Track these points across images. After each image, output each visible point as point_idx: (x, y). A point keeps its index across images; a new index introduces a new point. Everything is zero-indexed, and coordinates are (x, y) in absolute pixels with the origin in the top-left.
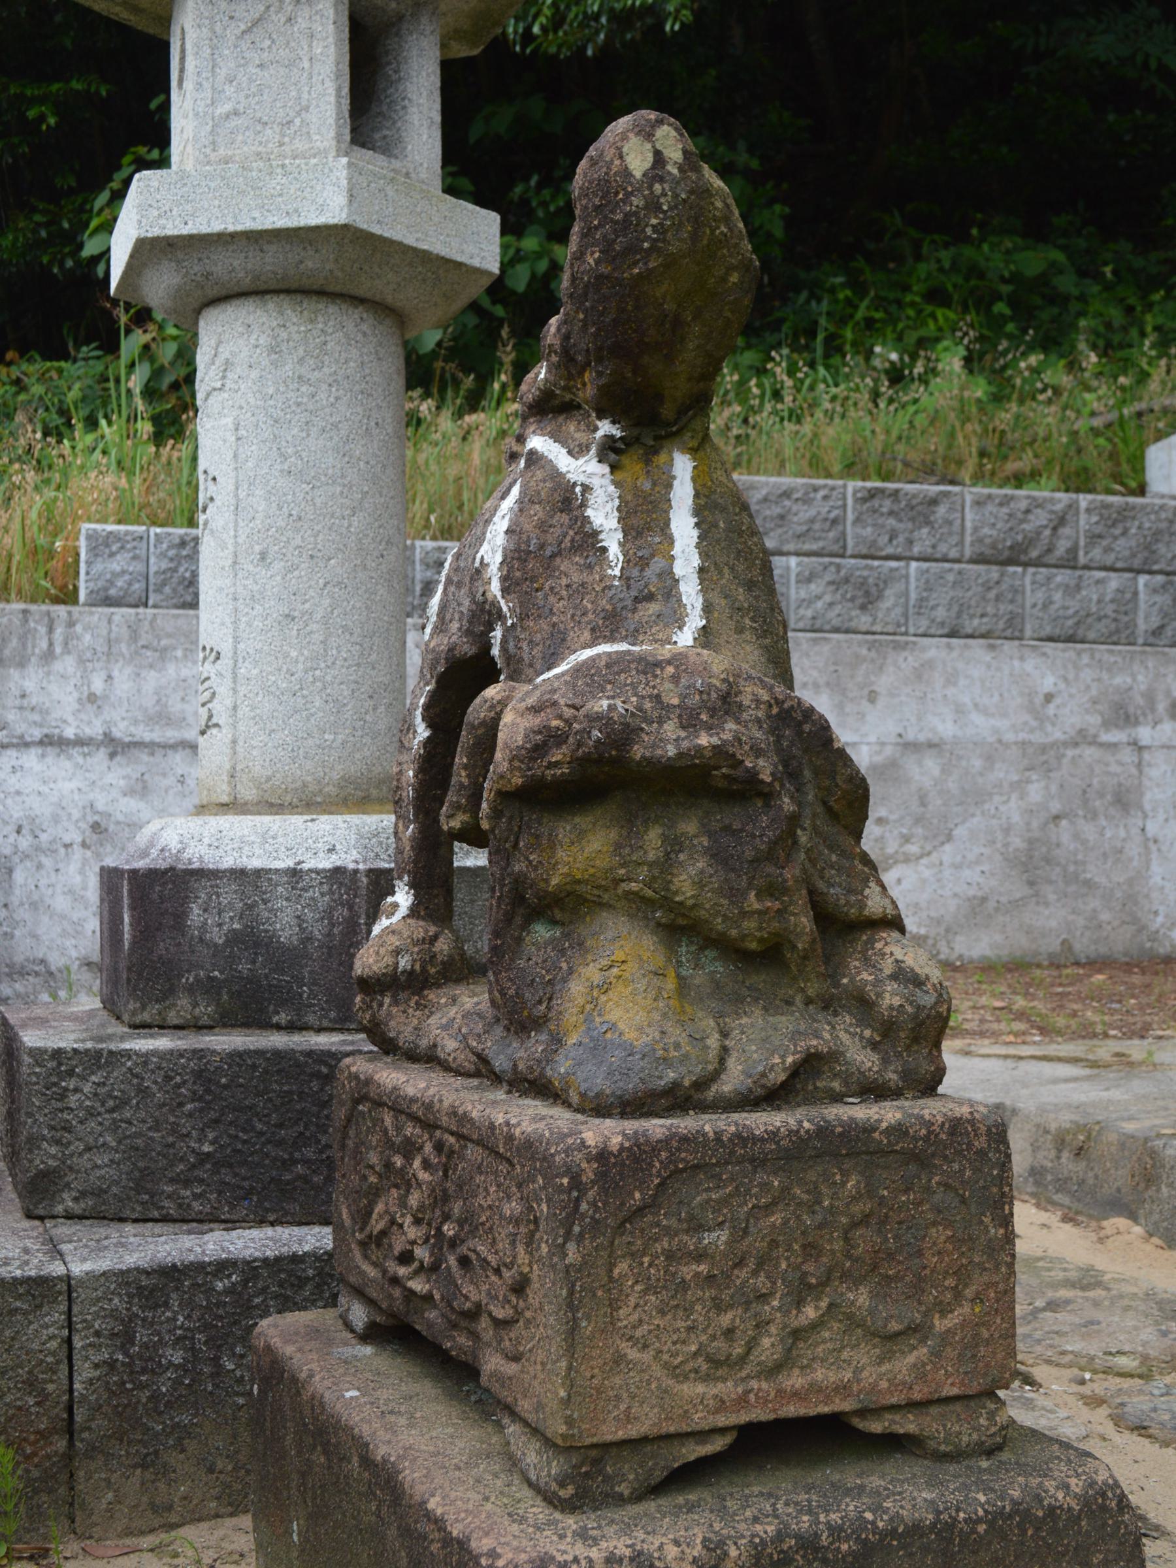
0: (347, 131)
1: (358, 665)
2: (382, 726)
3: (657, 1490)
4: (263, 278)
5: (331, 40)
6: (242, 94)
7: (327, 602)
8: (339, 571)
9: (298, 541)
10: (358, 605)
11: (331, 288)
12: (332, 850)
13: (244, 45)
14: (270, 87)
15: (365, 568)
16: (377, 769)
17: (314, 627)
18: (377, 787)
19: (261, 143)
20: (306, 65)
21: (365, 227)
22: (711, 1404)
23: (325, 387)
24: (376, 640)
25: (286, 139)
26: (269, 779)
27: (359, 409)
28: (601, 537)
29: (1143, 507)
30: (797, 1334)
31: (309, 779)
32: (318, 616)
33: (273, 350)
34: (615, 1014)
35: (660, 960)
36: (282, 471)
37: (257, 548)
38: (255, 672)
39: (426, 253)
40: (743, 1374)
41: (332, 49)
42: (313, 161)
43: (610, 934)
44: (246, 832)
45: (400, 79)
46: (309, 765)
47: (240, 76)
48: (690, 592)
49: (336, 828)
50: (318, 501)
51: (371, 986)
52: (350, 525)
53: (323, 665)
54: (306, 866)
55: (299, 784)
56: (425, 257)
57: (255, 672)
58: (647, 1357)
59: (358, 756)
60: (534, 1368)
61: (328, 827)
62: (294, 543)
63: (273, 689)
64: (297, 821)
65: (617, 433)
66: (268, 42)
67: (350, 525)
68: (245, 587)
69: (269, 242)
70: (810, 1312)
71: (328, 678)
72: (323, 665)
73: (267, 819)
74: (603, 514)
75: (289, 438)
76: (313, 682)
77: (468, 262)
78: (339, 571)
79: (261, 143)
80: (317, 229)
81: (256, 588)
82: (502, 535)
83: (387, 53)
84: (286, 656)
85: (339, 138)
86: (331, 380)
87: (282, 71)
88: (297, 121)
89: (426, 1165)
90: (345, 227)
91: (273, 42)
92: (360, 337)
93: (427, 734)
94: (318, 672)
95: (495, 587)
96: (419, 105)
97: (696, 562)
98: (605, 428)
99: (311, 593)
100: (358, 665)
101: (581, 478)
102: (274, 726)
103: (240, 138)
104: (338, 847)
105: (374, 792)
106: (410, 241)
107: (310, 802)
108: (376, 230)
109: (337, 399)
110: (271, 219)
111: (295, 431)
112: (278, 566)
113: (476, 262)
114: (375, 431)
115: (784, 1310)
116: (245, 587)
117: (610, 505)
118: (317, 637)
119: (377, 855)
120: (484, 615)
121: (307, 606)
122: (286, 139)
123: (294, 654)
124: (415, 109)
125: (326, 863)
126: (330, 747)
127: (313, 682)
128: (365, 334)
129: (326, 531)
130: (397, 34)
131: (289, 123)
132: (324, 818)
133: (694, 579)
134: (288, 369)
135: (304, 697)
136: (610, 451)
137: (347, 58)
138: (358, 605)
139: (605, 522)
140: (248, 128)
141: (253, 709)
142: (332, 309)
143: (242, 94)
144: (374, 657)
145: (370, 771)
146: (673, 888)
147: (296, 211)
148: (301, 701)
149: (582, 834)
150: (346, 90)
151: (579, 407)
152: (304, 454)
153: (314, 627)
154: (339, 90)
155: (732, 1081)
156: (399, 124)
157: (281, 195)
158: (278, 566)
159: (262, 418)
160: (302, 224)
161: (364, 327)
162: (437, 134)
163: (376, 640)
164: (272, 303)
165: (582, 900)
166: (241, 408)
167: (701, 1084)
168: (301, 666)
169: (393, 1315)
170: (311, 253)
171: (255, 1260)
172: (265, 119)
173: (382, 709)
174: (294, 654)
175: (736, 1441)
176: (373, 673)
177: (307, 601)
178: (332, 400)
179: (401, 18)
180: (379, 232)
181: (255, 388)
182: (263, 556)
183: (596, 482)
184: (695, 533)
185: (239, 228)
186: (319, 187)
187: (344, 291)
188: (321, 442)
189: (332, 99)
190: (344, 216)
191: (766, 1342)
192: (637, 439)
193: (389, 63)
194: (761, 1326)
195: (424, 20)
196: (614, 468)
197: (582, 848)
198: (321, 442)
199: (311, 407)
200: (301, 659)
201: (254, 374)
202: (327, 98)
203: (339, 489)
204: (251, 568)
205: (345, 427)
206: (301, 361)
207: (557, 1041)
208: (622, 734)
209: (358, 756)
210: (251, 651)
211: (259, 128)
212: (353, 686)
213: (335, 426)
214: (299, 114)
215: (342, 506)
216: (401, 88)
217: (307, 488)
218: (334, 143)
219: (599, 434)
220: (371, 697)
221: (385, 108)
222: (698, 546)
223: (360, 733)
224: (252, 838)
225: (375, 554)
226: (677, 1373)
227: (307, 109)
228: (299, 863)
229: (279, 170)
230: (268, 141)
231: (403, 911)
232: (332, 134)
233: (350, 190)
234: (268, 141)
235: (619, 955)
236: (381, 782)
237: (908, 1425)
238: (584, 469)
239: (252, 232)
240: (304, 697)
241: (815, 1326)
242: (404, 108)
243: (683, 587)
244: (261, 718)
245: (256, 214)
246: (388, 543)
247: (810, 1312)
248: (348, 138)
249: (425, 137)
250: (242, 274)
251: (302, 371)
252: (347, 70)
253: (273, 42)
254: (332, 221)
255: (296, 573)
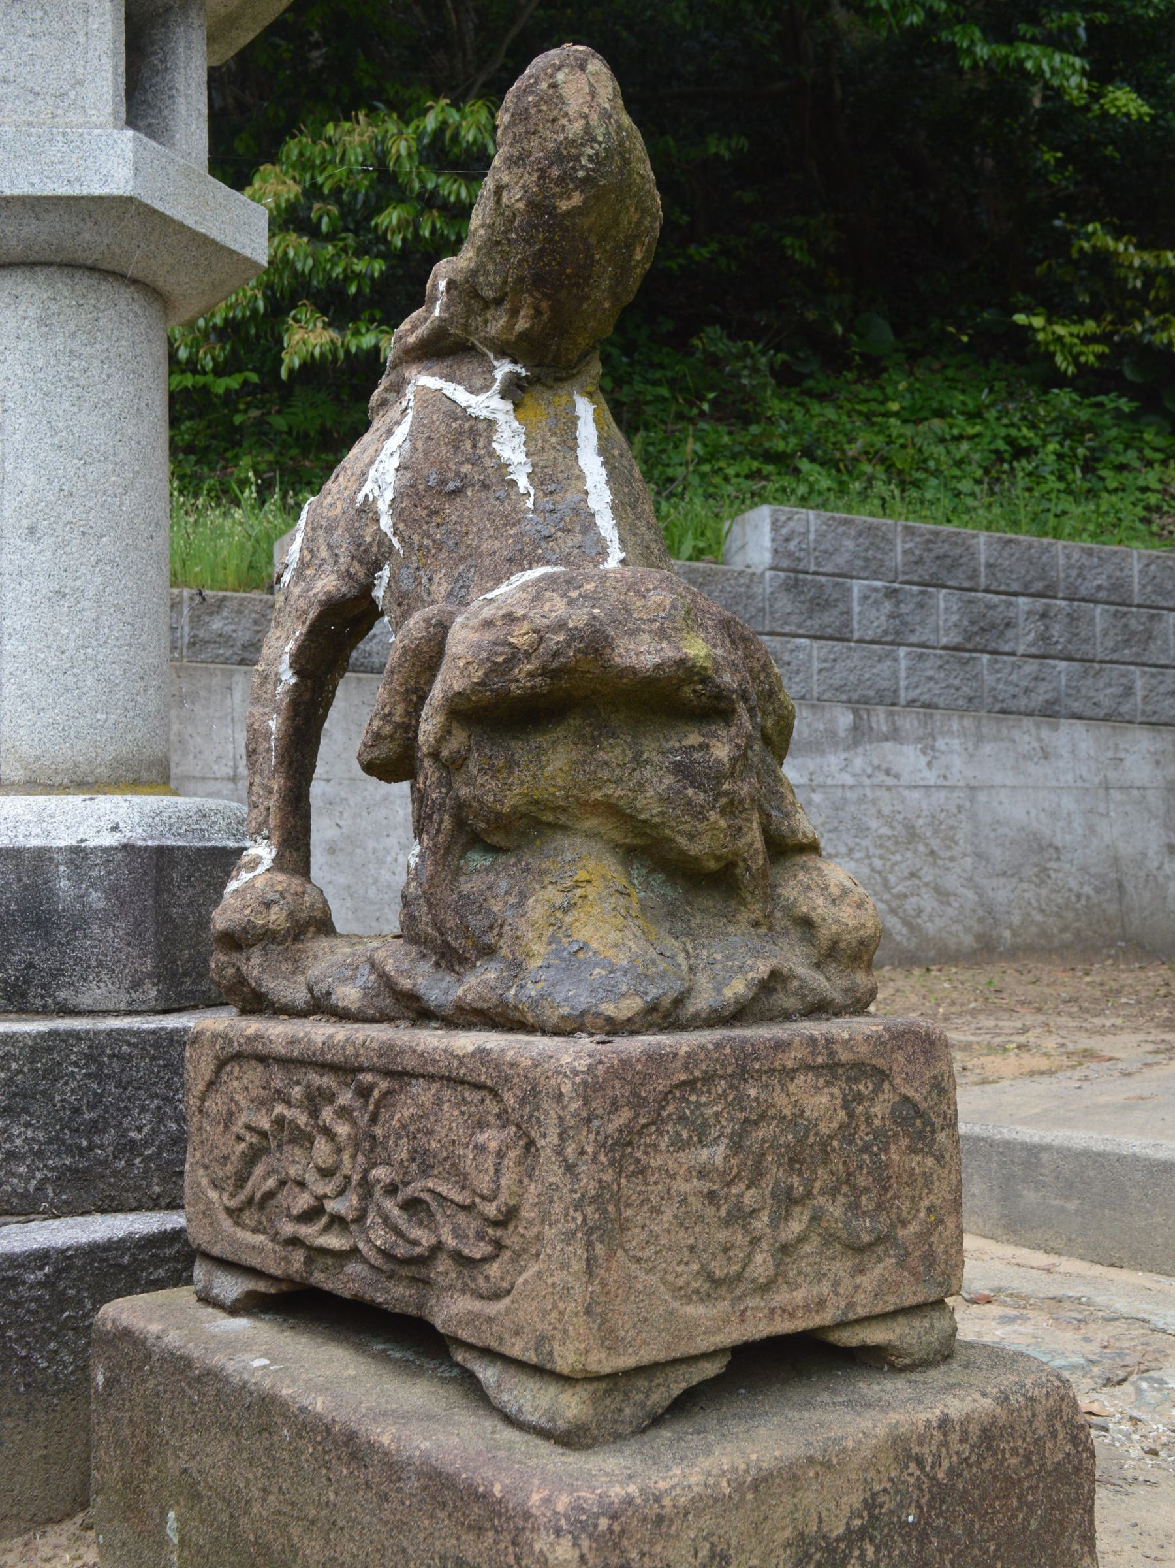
0: (123, 109)
1: (130, 645)
2: (152, 708)
3: (657, 1420)
4: (36, 248)
5: (108, 17)
6: (12, 63)
7: (98, 580)
8: (111, 549)
9: (69, 517)
10: (130, 584)
11: (104, 265)
12: (115, 828)
13: (15, 13)
14: (43, 58)
15: (136, 548)
16: (148, 752)
17: (87, 604)
18: (148, 770)
19: (32, 113)
20: (82, 40)
21: (149, 202)
22: (719, 1325)
23: (96, 363)
24: (147, 621)
25: (60, 112)
26: (38, 759)
27: (131, 389)
28: (510, 469)
29: (724, 573)
30: (785, 1249)
31: (81, 759)
32: (90, 593)
33: (42, 322)
34: (584, 934)
35: (621, 881)
36: (53, 445)
37: (25, 523)
38: (22, 649)
39: (205, 237)
40: (738, 1292)
41: (109, 26)
42: (97, 132)
43: (568, 856)
44: (20, 811)
45: (167, 69)
46: (81, 745)
47: (10, 44)
48: (606, 525)
49: (117, 806)
50: (90, 478)
51: (234, 941)
52: (122, 504)
53: (95, 643)
54: (91, 844)
55: (70, 763)
56: (203, 241)
57: (22, 649)
58: (654, 1279)
59: (129, 737)
60: (540, 1298)
61: (108, 806)
62: (65, 519)
63: (42, 666)
64: (75, 801)
65: (524, 373)
66: (40, 14)
67: (122, 504)
68: (11, 562)
69: (46, 211)
70: (796, 1227)
71: (100, 657)
72: (95, 643)
73: (42, 799)
74: (510, 447)
75: (60, 413)
76: (85, 661)
77: (241, 251)
78: (111, 549)
79: (32, 113)
80: (101, 198)
81: (23, 563)
82: (393, 472)
83: (152, 43)
84: (57, 633)
85: (115, 113)
86: (103, 357)
87: (55, 43)
88: (72, 94)
89: (344, 1113)
90: (130, 199)
91: (46, 13)
92: (131, 316)
93: (293, 681)
94: (90, 651)
95: (386, 523)
96: (187, 96)
97: (608, 498)
98: (503, 369)
99: (83, 569)
100: (130, 645)
101: (484, 413)
102: (43, 705)
103: (10, 106)
104: (122, 825)
105: (145, 775)
106: (189, 222)
107: (84, 784)
108: (158, 206)
109: (109, 376)
110: (52, 186)
111: (67, 405)
112: (48, 541)
113: (247, 252)
114: (146, 412)
115: (774, 1225)
116: (11, 562)
117: (517, 440)
118: (89, 615)
119: (161, 834)
120: (371, 558)
121: (78, 583)
122: (60, 112)
123: (65, 631)
124: (182, 100)
125: (110, 840)
126: (102, 726)
127: (85, 661)
128: (136, 314)
129: (98, 508)
130: (163, 25)
131: (62, 95)
132: (101, 797)
133: (608, 514)
134: (59, 342)
135: (75, 675)
136: (514, 391)
137: (123, 37)
138: (130, 584)
139: (512, 457)
140: (18, 97)
141: (20, 686)
142: (104, 286)
143: (12, 63)
144: (144, 638)
145: (141, 753)
146: (639, 806)
147: (78, 179)
148: (71, 680)
149: (540, 752)
150: (122, 69)
151: (473, 348)
152: (75, 430)
153: (87, 604)
154: (116, 67)
155: (700, 1003)
156: (166, 113)
157: (62, 163)
158: (48, 541)
159: (30, 390)
160: (85, 193)
161: (135, 307)
162: (204, 126)
163: (147, 621)
164: (41, 275)
165: (537, 823)
166: (7, 379)
167: (679, 1001)
168: (72, 644)
169: (288, 1279)
170: (89, 224)
171: (68, 1249)
172: (38, 89)
173: (151, 691)
174: (65, 631)
175: (729, 1366)
176: (144, 654)
177: (78, 578)
178: (104, 376)
179: (168, 9)
180: (161, 209)
181: (24, 360)
182: (32, 530)
183: (501, 417)
184: (604, 471)
185: (16, 192)
186: (103, 158)
187: (117, 269)
188: (93, 418)
189: (110, 76)
190: (129, 188)
191: (759, 1258)
192: (539, 380)
193: (156, 53)
194: (755, 1241)
195: (193, 13)
196: (517, 406)
197: (552, 765)
198: (93, 418)
199: (82, 382)
200: (73, 637)
201: (23, 345)
202: (104, 74)
203: (111, 466)
204: (18, 542)
205: (117, 406)
206: (73, 335)
207: (516, 967)
208: (595, 643)
209: (129, 737)
210: (18, 628)
211: (30, 97)
212: (125, 666)
213: (108, 403)
214: (73, 87)
215: (114, 484)
216: (168, 78)
217: (80, 464)
218: (111, 119)
219: (499, 374)
220: (142, 678)
221: (150, 96)
222: (607, 483)
223: (131, 714)
224: (28, 817)
225: (146, 534)
226: (685, 1294)
227: (81, 83)
228: (82, 841)
229: (60, 138)
230: (40, 112)
231: (267, 863)
232: (109, 110)
233: (135, 163)
234: (40, 112)
235: (582, 875)
236: (152, 764)
237: (876, 1335)
238: (487, 404)
239: (29, 197)
240: (75, 675)
241: (802, 1239)
242: (172, 97)
243: (598, 521)
244: (29, 696)
245: (36, 180)
246: (157, 524)
247: (796, 1227)
248: (124, 116)
249: (193, 127)
250: (14, 243)
251: (75, 345)
252: (123, 50)
253: (46, 13)
254: (116, 193)
255: (67, 549)
